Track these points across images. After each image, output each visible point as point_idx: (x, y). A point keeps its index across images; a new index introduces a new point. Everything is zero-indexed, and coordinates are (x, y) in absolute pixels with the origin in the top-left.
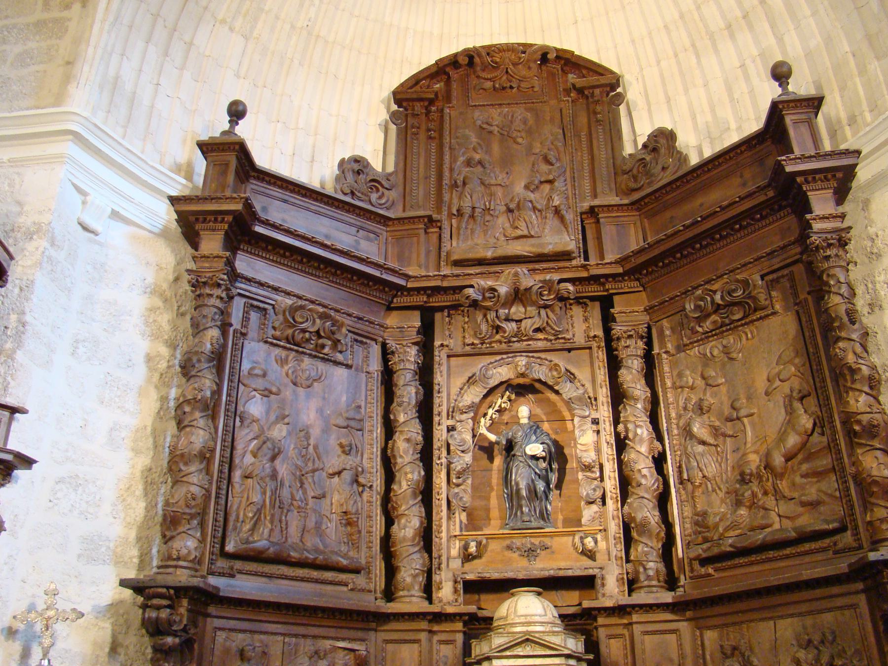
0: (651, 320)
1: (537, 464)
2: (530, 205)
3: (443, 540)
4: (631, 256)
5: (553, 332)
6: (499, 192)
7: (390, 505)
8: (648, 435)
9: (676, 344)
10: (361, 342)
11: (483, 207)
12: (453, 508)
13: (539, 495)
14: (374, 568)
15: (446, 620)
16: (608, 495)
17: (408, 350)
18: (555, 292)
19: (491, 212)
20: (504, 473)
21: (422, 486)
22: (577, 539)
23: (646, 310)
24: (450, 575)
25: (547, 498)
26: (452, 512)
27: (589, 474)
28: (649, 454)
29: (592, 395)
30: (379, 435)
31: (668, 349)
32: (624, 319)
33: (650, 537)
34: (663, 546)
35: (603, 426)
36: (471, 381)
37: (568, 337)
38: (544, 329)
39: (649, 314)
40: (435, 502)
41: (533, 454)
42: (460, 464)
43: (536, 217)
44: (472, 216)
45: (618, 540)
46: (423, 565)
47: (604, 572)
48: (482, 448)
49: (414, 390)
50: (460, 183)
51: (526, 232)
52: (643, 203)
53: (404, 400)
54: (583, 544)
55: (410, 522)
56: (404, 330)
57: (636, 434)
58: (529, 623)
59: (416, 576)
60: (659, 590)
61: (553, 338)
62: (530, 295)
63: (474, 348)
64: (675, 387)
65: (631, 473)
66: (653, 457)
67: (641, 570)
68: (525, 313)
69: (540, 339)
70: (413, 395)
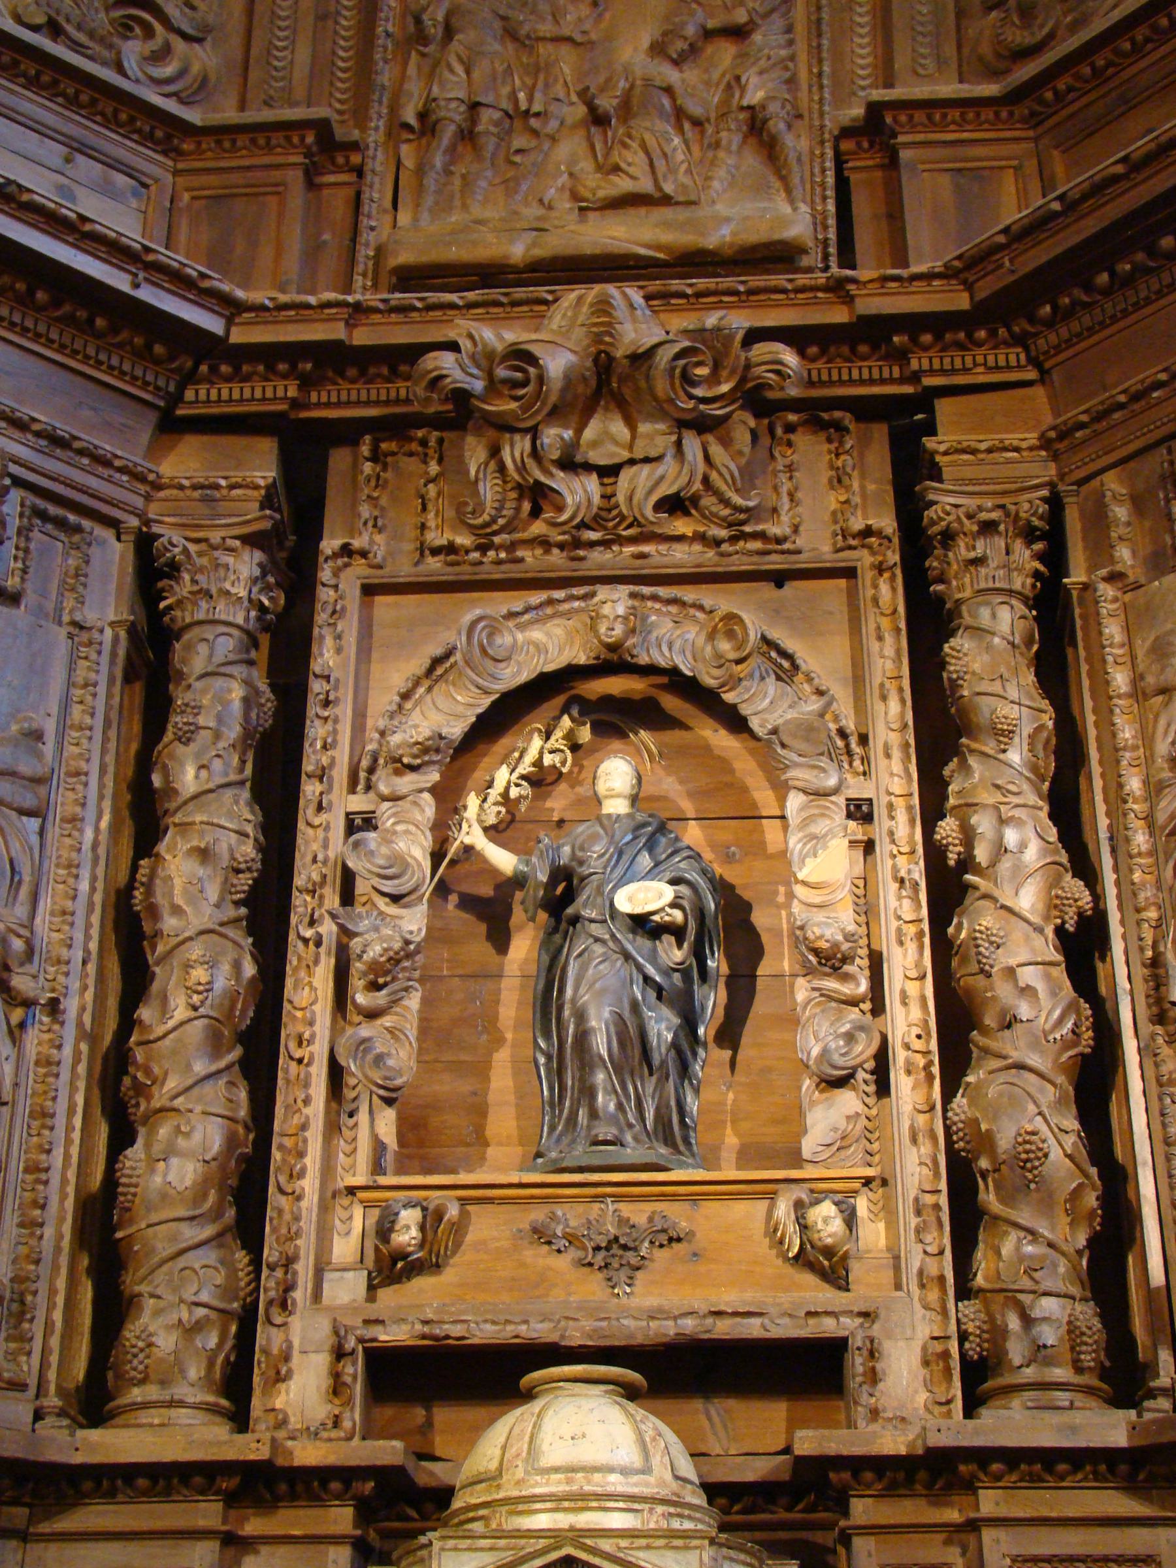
0: (1062, 476)
1: (655, 950)
2: (666, 102)
3: (304, 1204)
4: (1001, 248)
5: (726, 512)
6: (567, 64)
7: (127, 1081)
8: (1044, 852)
9: (1149, 549)
10: (61, 523)
11: (505, 104)
12: (349, 1094)
13: (656, 1060)
14: (41, 1300)
15: (293, 1497)
16: (899, 1057)
17: (230, 560)
18: (733, 372)
19: (534, 122)
20: (541, 986)
21: (245, 1016)
22: (783, 1209)
23: (1045, 443)
24: (322, 1329)
25: (684, 1070)
26: (348, 1107)
27: (831, 984)
28: (1047, 918)
29: (850, 725)
30: (103, 838)
31: (1119, 568)
32: (968, 473)
33: (1046, 1205)
34: (1091, 1243)
35: (887, 824)
36: (439, 671)
37: (775, 530)
38: (695, 500)
39: (1055, 457)
40: (286, 1069)
41: (638, 910)
42: (382, 939)
43: (686, 143)
44: (468, 135)
45: (932, 1219)
46: (228, 1291)
47: (876, 1330)
48: (469, 903)
49: (237, 693)
50: (436, 32)
51: (645, 185)
52: (1049, 95)
53: (201, 721)
54: (804, 1227)
55: (187, 1135)
56: (217, 494)
57: (1000, 850)
58: (580, 1500)
59: (198, 1327)
60: (1080, 1399)
61: (723, 533)
62: (648, 378)
63: (452, 564)
64: (1138, 693)
65: (980, 981)
66: (1060, 931)
67: (1014, 1323)
68: (631, 447)
69: (680, 538)
70: (237, 706)
